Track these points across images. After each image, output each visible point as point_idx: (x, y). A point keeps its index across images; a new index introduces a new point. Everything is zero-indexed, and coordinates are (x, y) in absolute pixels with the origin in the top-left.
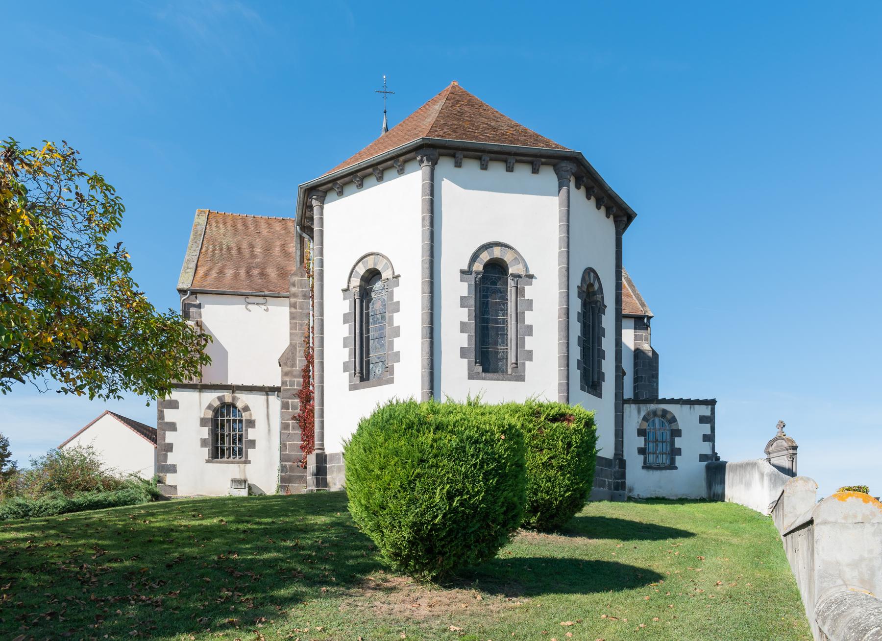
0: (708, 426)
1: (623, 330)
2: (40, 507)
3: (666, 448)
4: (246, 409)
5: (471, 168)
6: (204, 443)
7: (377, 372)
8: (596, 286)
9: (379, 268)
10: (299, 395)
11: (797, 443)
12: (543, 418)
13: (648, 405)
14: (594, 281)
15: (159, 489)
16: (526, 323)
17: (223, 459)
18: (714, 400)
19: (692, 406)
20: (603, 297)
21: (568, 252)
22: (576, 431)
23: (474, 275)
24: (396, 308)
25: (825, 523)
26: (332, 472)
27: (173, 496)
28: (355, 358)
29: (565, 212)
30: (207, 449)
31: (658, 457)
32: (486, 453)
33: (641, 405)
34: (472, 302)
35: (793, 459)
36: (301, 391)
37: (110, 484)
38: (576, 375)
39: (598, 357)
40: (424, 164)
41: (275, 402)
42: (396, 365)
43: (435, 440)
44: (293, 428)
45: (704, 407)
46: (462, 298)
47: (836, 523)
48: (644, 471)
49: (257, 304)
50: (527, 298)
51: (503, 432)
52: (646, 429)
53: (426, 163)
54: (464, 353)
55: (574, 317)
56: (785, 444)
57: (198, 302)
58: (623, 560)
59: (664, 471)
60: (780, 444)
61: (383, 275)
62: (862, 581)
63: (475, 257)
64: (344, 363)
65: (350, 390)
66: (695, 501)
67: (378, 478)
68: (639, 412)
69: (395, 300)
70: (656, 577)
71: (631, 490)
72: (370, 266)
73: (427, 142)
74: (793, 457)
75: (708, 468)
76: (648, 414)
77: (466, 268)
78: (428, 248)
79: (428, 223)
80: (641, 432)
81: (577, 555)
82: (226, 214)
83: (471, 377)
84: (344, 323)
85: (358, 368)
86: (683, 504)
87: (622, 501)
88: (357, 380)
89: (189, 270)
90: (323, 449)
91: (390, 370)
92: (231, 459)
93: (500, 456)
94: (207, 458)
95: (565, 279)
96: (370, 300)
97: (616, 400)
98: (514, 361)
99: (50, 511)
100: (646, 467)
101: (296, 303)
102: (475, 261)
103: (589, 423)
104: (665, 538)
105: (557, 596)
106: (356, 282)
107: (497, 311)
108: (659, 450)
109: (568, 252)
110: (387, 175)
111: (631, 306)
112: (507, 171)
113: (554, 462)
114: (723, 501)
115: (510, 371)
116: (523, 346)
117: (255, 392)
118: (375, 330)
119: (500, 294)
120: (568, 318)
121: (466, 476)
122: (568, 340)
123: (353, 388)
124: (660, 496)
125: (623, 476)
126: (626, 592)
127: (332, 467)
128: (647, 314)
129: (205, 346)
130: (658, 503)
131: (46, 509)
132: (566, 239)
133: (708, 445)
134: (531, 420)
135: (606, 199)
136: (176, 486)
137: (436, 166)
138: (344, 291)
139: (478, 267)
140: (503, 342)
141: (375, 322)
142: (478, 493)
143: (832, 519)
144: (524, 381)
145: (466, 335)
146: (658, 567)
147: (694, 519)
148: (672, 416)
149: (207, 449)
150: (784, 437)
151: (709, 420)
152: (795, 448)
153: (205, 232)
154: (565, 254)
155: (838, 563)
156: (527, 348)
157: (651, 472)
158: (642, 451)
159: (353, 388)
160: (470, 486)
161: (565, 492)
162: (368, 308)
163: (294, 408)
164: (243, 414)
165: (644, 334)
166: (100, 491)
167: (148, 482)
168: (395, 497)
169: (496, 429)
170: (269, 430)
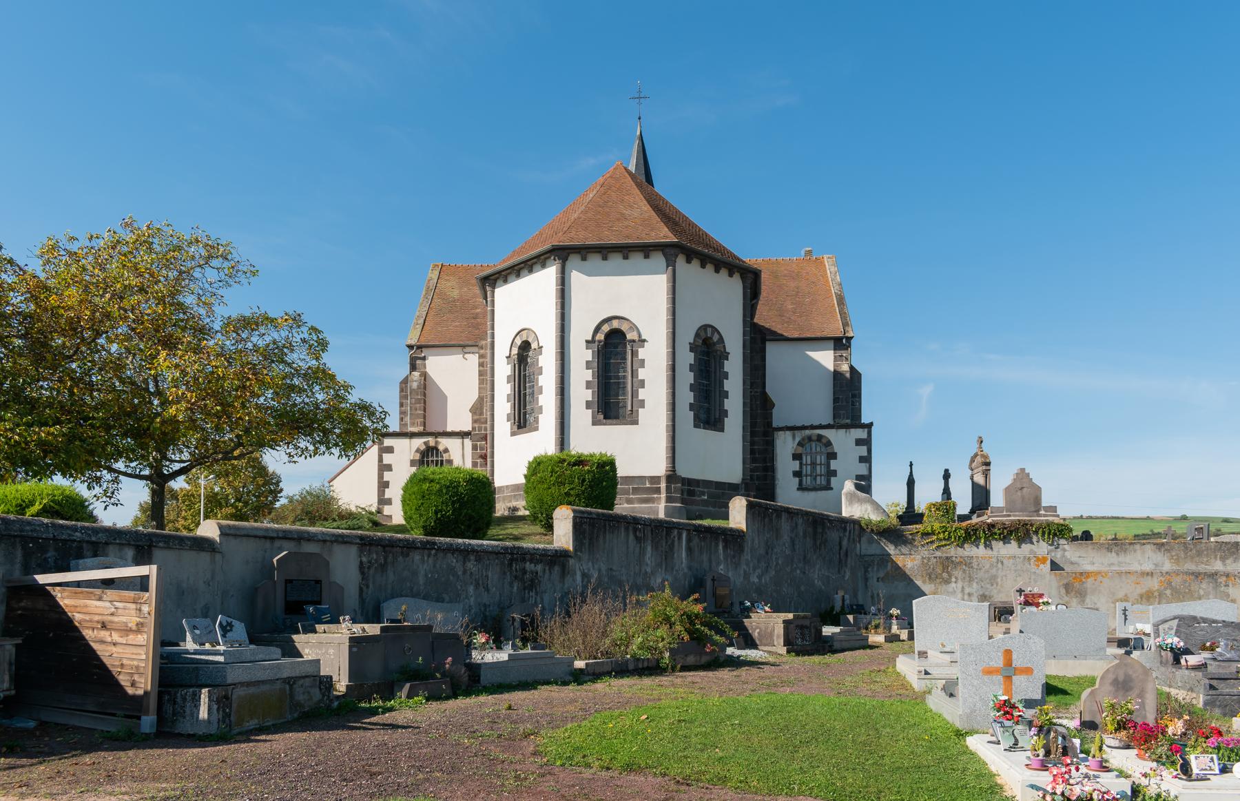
0: (865, 448)
4: (446, 450)
5: (595, 260)
11: (992, 459)
12: (566, 464)
13: (803, 432)
15: (378, 518)
16: (639, 378)
19: (848, 430)
23: (597, 343)
26: (499, 501)
28: (515, 410)
33: (796, 432)
34: (596, 364)
35: (987, 475)
37: (350, 516)
39: (720, 397)
41: (468, 442)
43: (429, 487)
48: (799, 493)
49: (473, 353)
53: (557, 261)
54: (588, 405)
57: (423, 355)
59: (819, 492)
64: (508, 415)
74: (986, 474)
77: (590, 338)
80: (796, 457)
82: (457, 265)
83: (594, 424)
89: (418, 326)
91: (537, 420)
95: (671, 341)
100: (801, 488)
101: (484, 362)
102: (597, 332)
106: (515, 351)
117: (453, 437)
118: (530, 387)
123: (513, 434)
128: (846, 335)
129: (385, 418)
136: (391, 516)
138: (507, 357)
139: (601, 337)
142: (449, 511)
144: (638, 424)
152: (988, 464)
153: (436, 286)
157: (806, 493)
158: (797, 474)
160: (445, 508)
162: (525, 370)
164: (444, 455)
166: (336, 521)
167: (371, 513)
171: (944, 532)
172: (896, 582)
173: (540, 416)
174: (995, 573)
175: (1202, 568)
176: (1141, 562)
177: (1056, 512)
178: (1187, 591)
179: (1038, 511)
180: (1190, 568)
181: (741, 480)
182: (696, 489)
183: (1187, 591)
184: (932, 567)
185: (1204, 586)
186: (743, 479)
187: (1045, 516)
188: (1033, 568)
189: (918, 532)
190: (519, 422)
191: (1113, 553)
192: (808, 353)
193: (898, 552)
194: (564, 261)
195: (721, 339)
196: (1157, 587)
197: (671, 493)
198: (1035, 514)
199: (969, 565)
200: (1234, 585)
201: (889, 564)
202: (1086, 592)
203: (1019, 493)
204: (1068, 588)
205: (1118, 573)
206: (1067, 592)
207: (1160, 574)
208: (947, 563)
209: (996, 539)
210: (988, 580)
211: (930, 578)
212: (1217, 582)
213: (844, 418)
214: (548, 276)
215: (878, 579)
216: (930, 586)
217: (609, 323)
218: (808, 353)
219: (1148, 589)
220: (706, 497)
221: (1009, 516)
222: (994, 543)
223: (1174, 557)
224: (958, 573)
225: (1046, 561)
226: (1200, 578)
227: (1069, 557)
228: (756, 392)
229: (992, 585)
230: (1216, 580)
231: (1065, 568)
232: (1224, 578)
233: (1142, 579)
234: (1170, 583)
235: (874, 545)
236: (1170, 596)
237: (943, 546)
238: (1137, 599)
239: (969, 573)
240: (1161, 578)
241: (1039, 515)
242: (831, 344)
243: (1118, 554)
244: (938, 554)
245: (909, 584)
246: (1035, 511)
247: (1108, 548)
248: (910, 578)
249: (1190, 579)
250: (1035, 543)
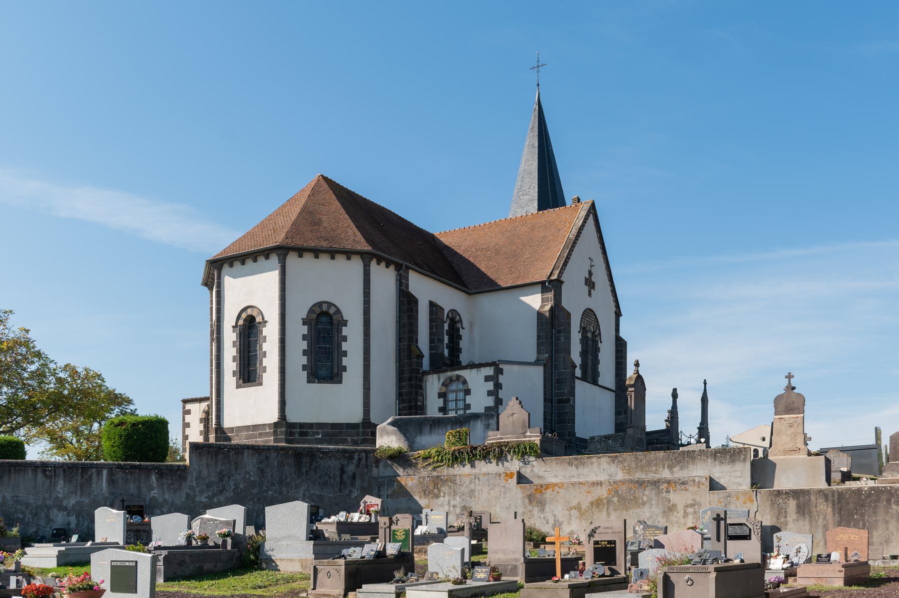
13: (446, 373)
23: (239, 327)
33: (441, 374)
34: (238, 343)
45: (488, 368)
68: (439, 380)
76: (446, 380)
77: (234, 325)
102: (239, 319)
139: (241, 322)
148: (464, 379)
165: (550, 296)
171: (438, 456)
172: (400, 498)
174: (473, 488)
175: (651, 476)
176: (598, 473)
178: (632, 497)
180: (640, 477)
182: (309, 430)
183: (632, 497)
184: (426, 484)
185: (647, 493)
186: (363, 419)
187: (530, 437)
188: (503, 482)
191: (573, 466)
192: (523, 298)
193: (405, 474)
195: (338, 311)
196: (605, 495)
197: (278, 436)
198: (522, 435)
199: (454, 482)
200: (675, 491)
201: (396, 483)
202: (545, 501)
204: (531, 498)
205: (572, 484)
206: (530, 502)
207: (608, 484)
208: (438, 482)
210: (468, 494)
211: (425, 494)
212: (659, 489)
213: (544, 353)
215: (388, 495)
216: (425, 500)
218: (523, 298)
219: (598, 498)
220: (320, 436)
221: (502, 438)
222: (477, 462)
223: (626, 468)
224: (445, 489)
225: (513, 475)
226: (644, 486)
227: (537, 472)
228: (404, 345)
229: (471, 498)
230: (658, 487)
231: (533, 481)
232: (666, 485)
233: (592, 489)
234: (617, 492)
235: (389, 468)
236: (617, 503)
237: (437, 467)
238: (589, 507)
239: (454, 489)
240: (609, 487)
241: (525, 437)
242: (539, 288)
243: (577, 467)
244: (435, 474)
245: (409, 499)
246: (523, 433)
247: (569, 463)
248: (410, 494)
249: (635, 487)
250: (509, 461)
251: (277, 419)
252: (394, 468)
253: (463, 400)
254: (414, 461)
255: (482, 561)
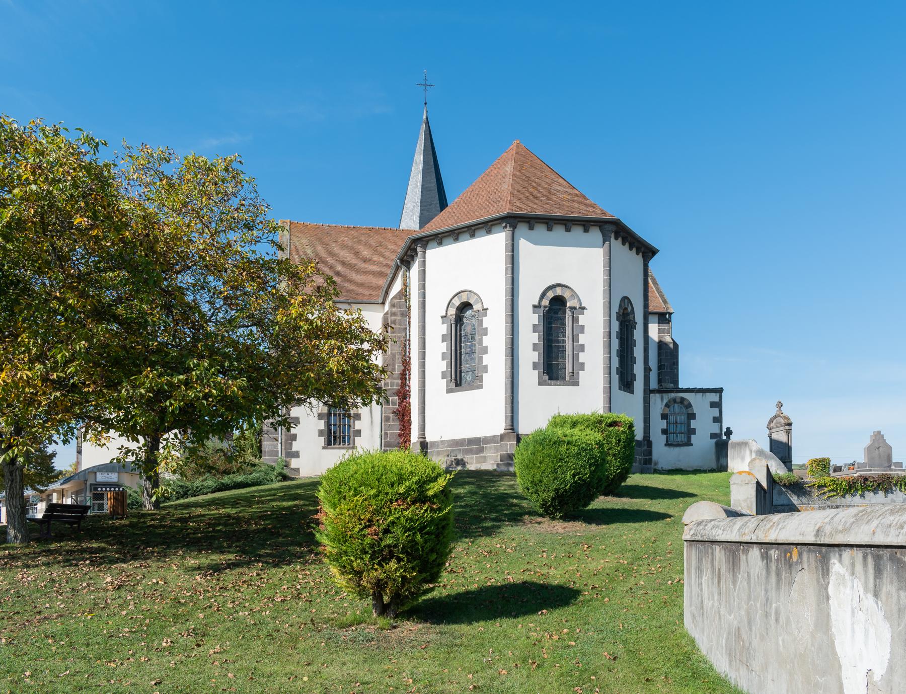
0: (717, 410)
1: (649, 325)
2: (197, 488)
3: (684, 429)
5: (540, 230)
6: (321, 433)
7: (468, 379)
8: (629, 309)
9: (471, 302)
10: (398, 393)
11: (792, 420)
12: (603, 425)
13: (669, 394)
14: (628, 306)
15: (286, 471)
16: (580, 343)
17: (335, 446)
18: (722, 388)
20: (634, 317)
21: (610, 290)
22: (624, 432)
23: (542, 308)
24: (485, 332)
25: (734, 484)
27: (297, 477)
29: (608, 260)
30: (323, 438)
31: (677, 436)
32: (590, 455)
33: (664, 394)
34: (541, 328)
36: (399, 390)
38: (616, 378)
39: (631, 362)
40: (507, 229)
42: (484, 375)
43: (567, 450)
44: (393, 420)
46: (534, 326)
47: (738, 484)
48: (667, 448)
50: (580, 324)
51: (597, 444)
52: (667, 414)
53: (508, 228)
54: (535, 366)
55: (614, 335)
56: (782, 421)
58: (652, 509)
59: (682, 448)
60: (779, 421)
61: (474, 307)
62: (748, 507)
63: (543, 295)
64: (442, 372)
65: (447, 393)
66: (705, 472)
67: (539, 467)
68: (662, 399)
69: (484, 326)
70: (670, 516)
71: (656, 464)
72: (464, 300)
73: (510, 215)
74: (788, 432)
75: (717, 444)
76: (669, 401)
78: (510, 290)
79: (510, 272)
80: (664, 416)
81: (626, 507)
83: (540, 384)
84: (443, 341)
85: (453, 376)
86: (695, 474)
87: (649, 474)
88: (453, 385)
90: (425, 438)
91: (480, 379)
92: (341, 446)
93: (596, 456)
94: (323, 445)
95: (608, 310)
96: (462, 324)
97: (644, 394)
98: (571, 371)
99: (205, 490)
100: (668, 444)
101: (395, 320)
103: (631, 426)
104: (678, 497)
105: (621, 524)
106: (452, 311)
107: (558, 333)
108: (679, 430)
109: (610, 290)
110: (477, 233)
111: (656, 304)
112: (566, 231)
113: (611, 452)
114: (727, 471)
115: (568, 379)
116: (578, 359)
118: (466, 347)
119: (560, 321)
120: (610, 338)
121: (581, 466)
122: (610, 355)
123: (449, 391)
124: (678, 467)
125: (650, 453)
126: (654, 522)
127: (431, 452)
128: (669, 311)
130: (676, 474)
131: (201, 489)
132: (608, 280)
133: (717, 425)
134: (597, 426)
135: (636, 244)
136: (299, 469)
137: (516, 230)
138: (442, 317)
139: (546, 302)
140: (563, 357)
141: (467, 341)
142: (586, 474)
143: (737, 482)
145: (537, 353)
146: (670, 512)
147: (700, 486)
149: (323, 438)
150: (782, 415)
151: (717, 405)
152: (790, 424)
154: (608, 292)
155: (739, 500)
156: (581, 361)
157: (672, 448)
158: (664, 432)
159: (449, 391)
161: (617, 470)
162: (460, 331)
163: (394, 404)
168: (548, 476)
169: (593, 443)
170: (372, 422)
173: (484, 375)
177: (902, 467)
179: (890, 466)
181: (642, 437)
187: (895, 470)
189: (815, 484)
190: (456, 380)
193: (800, 502)
194: (514, 227)
198: (888, 469)
203: (877, 452)
209: (869, 490)
214: (498, 240)
217: (553, 289)
221: (871, 470)
222: (866, 493)
235: (783, 496)
237: (832, 496)
241: (891, 470)
251: (504, 431)
252: (789, 495)
253: (670, 423)
254: (809, 489)
255: (714, 586)
